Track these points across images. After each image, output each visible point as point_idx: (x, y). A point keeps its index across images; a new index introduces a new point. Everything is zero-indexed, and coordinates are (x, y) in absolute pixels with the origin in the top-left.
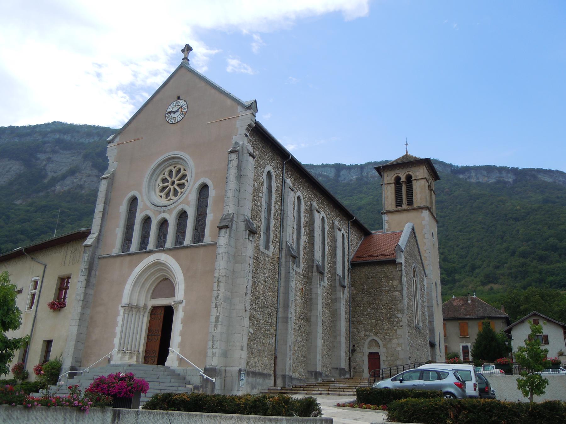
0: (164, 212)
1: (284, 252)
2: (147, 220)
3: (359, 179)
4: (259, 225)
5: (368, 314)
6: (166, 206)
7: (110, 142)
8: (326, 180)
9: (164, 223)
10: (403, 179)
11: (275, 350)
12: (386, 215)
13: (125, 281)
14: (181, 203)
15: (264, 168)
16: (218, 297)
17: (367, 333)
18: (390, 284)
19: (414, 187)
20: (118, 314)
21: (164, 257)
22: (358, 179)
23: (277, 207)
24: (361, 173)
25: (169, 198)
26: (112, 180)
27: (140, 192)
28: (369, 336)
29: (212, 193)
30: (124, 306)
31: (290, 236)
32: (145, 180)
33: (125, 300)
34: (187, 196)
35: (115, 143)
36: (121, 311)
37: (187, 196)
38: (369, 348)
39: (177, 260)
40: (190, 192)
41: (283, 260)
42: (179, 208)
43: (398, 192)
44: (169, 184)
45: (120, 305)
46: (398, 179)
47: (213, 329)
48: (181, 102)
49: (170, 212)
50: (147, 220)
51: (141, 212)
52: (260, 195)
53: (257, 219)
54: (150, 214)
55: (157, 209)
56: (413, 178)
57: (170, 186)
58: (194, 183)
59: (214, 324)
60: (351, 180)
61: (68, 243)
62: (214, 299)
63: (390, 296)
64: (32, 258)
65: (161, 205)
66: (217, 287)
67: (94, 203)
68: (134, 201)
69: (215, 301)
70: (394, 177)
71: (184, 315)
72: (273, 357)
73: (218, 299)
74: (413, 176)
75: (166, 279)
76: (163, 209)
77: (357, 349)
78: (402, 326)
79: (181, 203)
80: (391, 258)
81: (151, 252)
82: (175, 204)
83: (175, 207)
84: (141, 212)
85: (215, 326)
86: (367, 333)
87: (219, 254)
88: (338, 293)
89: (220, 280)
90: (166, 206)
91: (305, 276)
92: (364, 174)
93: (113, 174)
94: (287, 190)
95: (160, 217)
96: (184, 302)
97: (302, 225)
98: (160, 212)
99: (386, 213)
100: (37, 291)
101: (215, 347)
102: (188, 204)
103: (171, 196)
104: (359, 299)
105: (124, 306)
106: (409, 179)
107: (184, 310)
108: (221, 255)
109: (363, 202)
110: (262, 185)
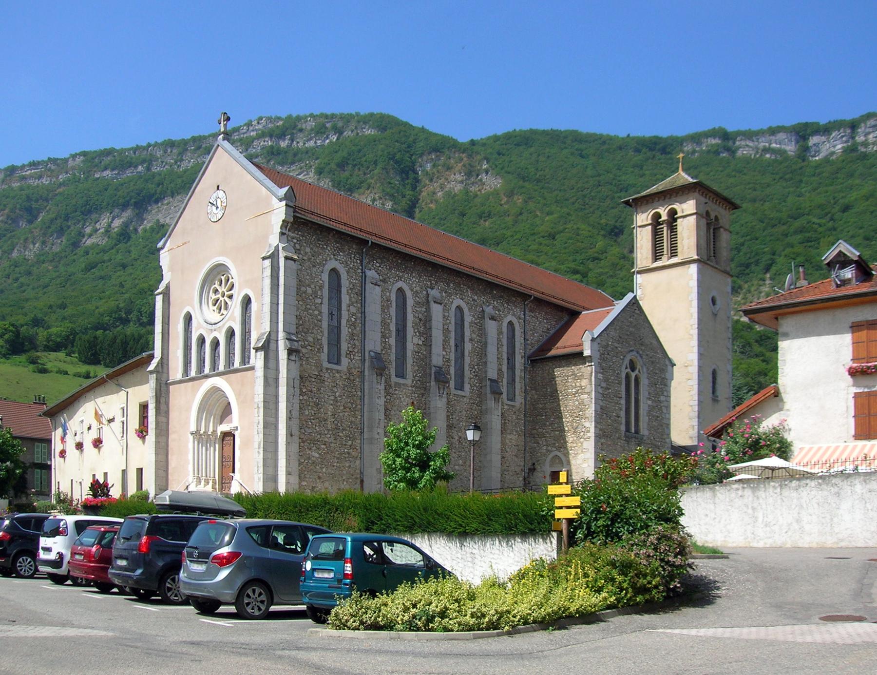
1: (367, 364)
2: (202, 340)
3: (852, 150)
4: (319, 337)
5: (551, 424)
8: (779, 157)
9: (216, 344)
10: (664, 217)
11: (361, 473)
12: (639, 276)
15: (324, 265)
17: (550, 448)
18: (578, 384)
19: (679, 229)
21: (219, 382)
22: (845, 151)
23: (353, 310)
24: (853, 138)
26: (166, 294)
27: (193, 308)
28: (551, 451)
31: (374, 342)
35: (166, 249)
37: (233, 312)
38: (551, 466)
41: (366, 373)
42: (227, 326)
43: (656, 235)
44: (219, 296)
46: (657, 216)
48: (220, 193)
50: (202, 340)
52: (319, 301)
53: (315, 332)
55: (210, 327)
56: (679, 215)
58: (239, 295)
60: (833, 153)
62: (255, 425)
63: (577, 400)
64: (118, 385)
65: (213, 322)
67: (152, 322)
68: (188, 319)
70: (650, 216)
72: (359, 481)
74: (679, 210)
76: (214, 327)
77: (538, 467)
80: (578, 349)
81: (207, 377)
83: (224, 325)
86: (550, 448)
88: (488, 402)
91: (417, 387)
92: (860, 139)
93: (168, 287)
94: (369, 286)
95: (212, 337)
97: (409, 324)
99: (639, 272)
100: (125, 419)
103: (223, 311)
104: (541, 406)
106: (673, 213)
109: (854, 195)
110: (321, 287)
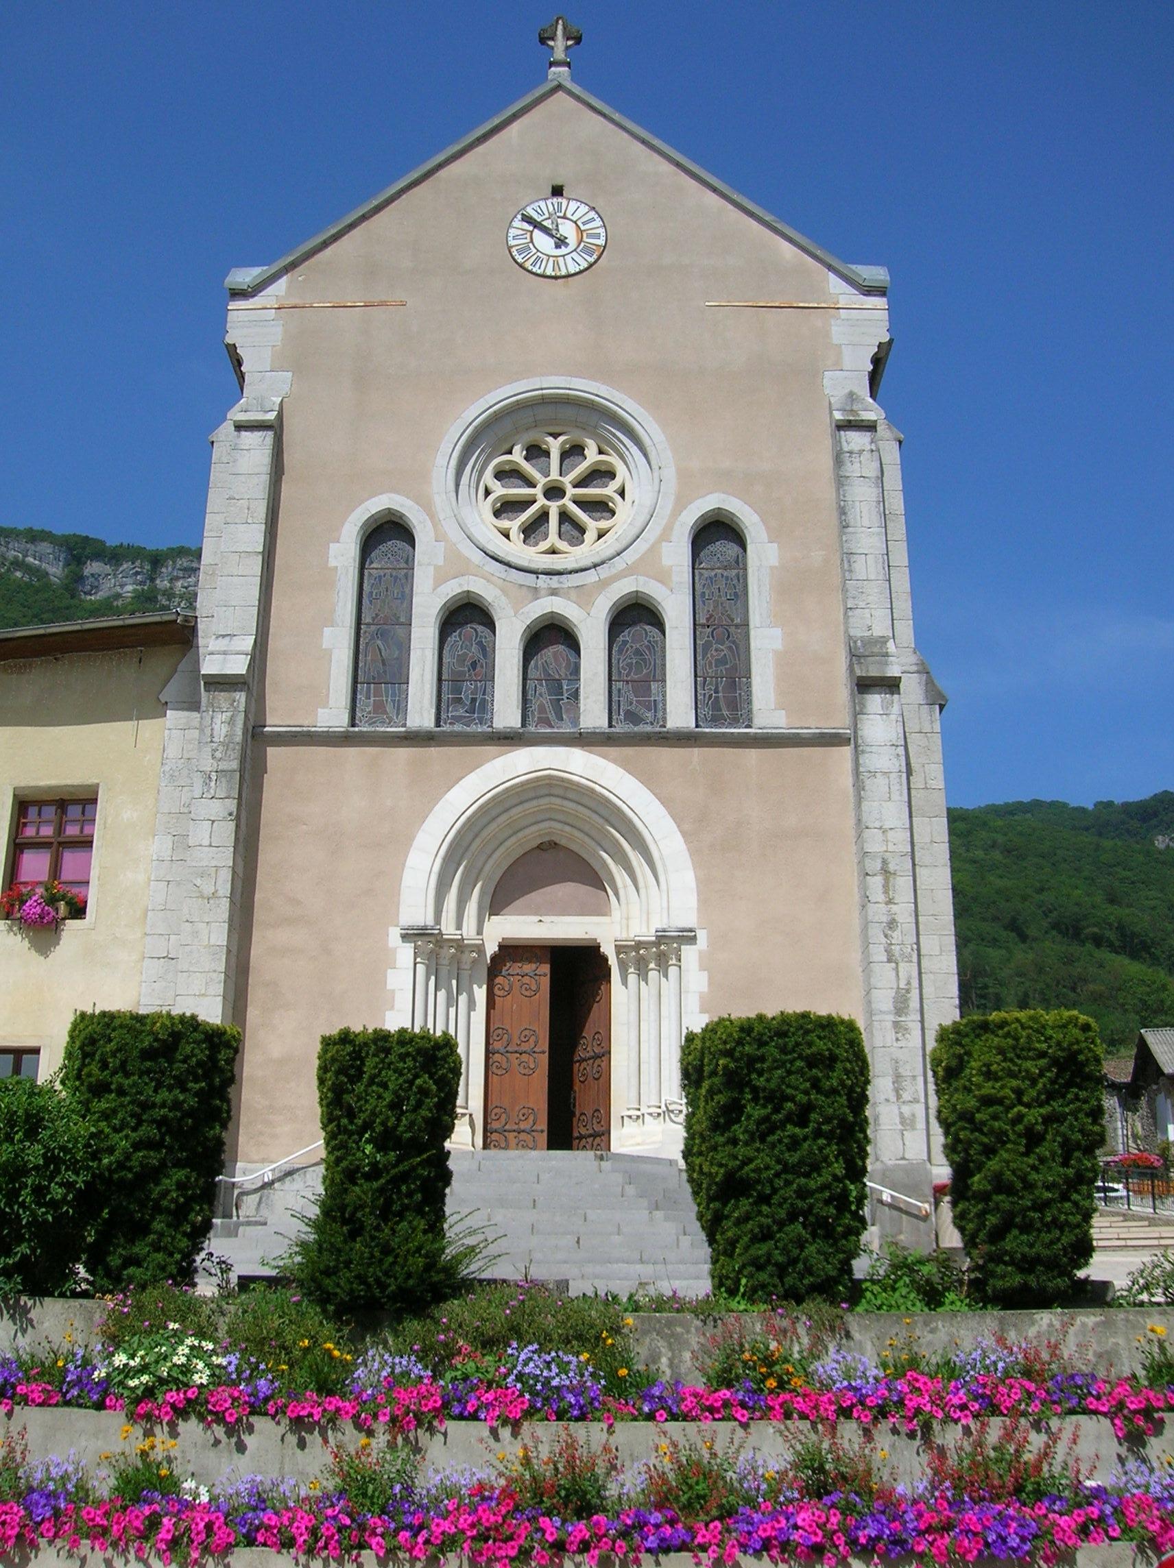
0: (554, 592)
6: (559, 573)
7: (239, 294)
13: (402, 842)
14: (630, 571)
16: (892, 924)
20: (387, 960)
25: (504, 524)
29: (763, 555)
30: (410, 935)
32: (441, 460)
33: (415, 908)
34: (654, 550)
36: (405, 953)
39: (648, 779)
40: (665, 536)
45: (394, 934)
47: (891, 1035)
49: (584, 596)
50: (466, 615)
51: (439, 581)
54: (488, 592)
57: (538, 491)
59: (892, 1018)
61: (594, 733)
66: (886, 892)
68: (387, 533)
69: (884, 940)
71: (711, 983)
73: (896, 935)
75: (553, 845)
78: (497, 1438)
79: (630, 571)
82: (604, 572)
83: (604, 584)
84: (439, 581)
85: (896, 1024)
87: (873, 774)
89: (891, 867)
90: (559, 573)
96: (702, 936)
98: (535, 592)
101: (906, 1096)
102: (663, 577)
103: (515, 524)
105: (410, 935)
107: (706, 964)
108: (881, 781)
